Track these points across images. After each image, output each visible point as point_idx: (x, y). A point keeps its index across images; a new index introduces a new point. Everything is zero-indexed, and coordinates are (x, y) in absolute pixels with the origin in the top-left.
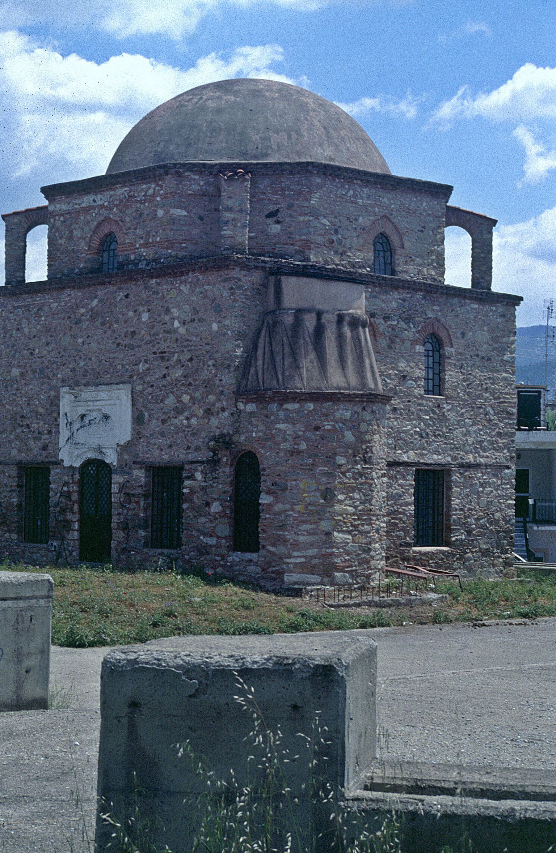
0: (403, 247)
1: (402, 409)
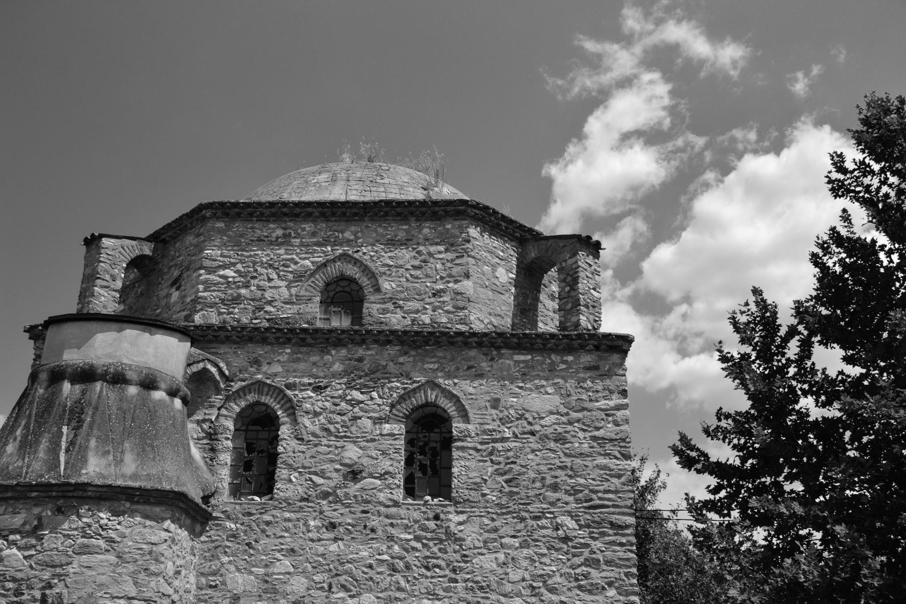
0: (377, 289)
1: (349, 524)
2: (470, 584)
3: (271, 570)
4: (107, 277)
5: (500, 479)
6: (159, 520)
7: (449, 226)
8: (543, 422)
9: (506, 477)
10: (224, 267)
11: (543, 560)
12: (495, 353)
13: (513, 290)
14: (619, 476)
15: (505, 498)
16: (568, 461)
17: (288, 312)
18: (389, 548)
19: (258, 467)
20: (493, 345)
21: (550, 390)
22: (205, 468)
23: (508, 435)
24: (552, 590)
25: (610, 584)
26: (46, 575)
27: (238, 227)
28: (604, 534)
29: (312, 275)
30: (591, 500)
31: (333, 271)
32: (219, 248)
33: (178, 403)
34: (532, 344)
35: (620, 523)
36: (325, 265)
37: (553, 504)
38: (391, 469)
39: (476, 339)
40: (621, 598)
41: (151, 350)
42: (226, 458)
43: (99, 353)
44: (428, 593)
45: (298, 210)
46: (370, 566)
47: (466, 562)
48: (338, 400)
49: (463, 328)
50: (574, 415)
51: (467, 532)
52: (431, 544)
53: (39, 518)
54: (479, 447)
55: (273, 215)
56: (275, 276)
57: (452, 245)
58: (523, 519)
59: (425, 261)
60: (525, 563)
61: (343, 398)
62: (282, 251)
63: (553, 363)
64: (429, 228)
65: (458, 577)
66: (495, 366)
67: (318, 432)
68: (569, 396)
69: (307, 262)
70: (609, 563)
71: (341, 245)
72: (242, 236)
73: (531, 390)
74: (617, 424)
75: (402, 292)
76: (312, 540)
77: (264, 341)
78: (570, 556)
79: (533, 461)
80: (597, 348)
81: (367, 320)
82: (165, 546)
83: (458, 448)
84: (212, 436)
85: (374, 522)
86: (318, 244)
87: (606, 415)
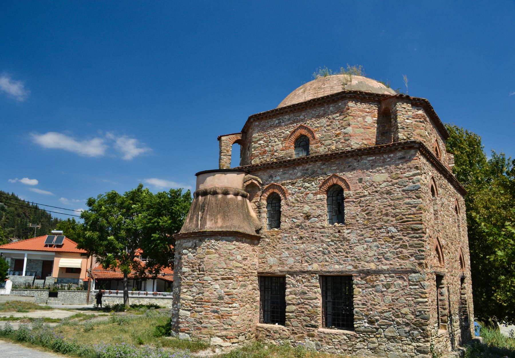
0: (314, 138)
2: (353, 258)
3: (281, 256)
4: (225, 151)
5: (364, 213)
6: (231, 241)
7: (340, 104)
8: (381, 186)
9: (366, 212)
10: (259, 140)
11: (382, 246)
12: (359, 158)
13: (376, 125)
14: (415, 207)
15: (366, 221)
16: (392, 202)
17: (282, 154)
18: (322, 245)
19: (276, 219)
20: (357, 155)
21: (383, 171)
22: (257, 220)
23: (366, 194)
24: (387, 259)
25: (412, 255)
26: (199, 262)
27: (263, 123)
28: (409, 234)
29: (290, 137)
30: (403, 219)
31: (297, 134)
32: (257, 133)
33: (239, 198)
34: (374, 152)
35: (415, 228)
36: (294, 132)
37: (386, 222)
38: (321, 213)
39: (350, 154)
40: (417, 261)
41: (226, 180)
42: (265, 215)
43: (208, 184)
44: (337, 262)
45: (282, 111)
46: (315, 253)
47: (351, 249)
48: (300, 188)
49: (349, 149)
50: (395, 181)
51: (351, 237)
52: (338, 243)
53: (196, 243)
54: (355, 200)
55: (274, 115)
56: (277, 140)
57: (342, 112)
58: (374, 230)
59: (331, 122)
60: (375, 248)
61: (302, 186)
62: (279, 129)
63: (384, 159)
64: (332, 107)
65: (348, 256)
66: (360, 164)
67: (294, 201)
68: (392, 173)
69: (288, 132)
70: (411, 246)
71: (299, 122)
72: (264, 126)
73: (375, 172)
74: (414, 183)
75: (323, 137)
76: (294, 244)
77: (272, 168)
78: (394, 244)
79: (377, 204)
80: (403, 148)
81: (311, 152)
82: (234, 250)
83: (346, 202)
84: (259, 207)
85: (316, 235)
86: (291, 123)
87: (409, 179)
